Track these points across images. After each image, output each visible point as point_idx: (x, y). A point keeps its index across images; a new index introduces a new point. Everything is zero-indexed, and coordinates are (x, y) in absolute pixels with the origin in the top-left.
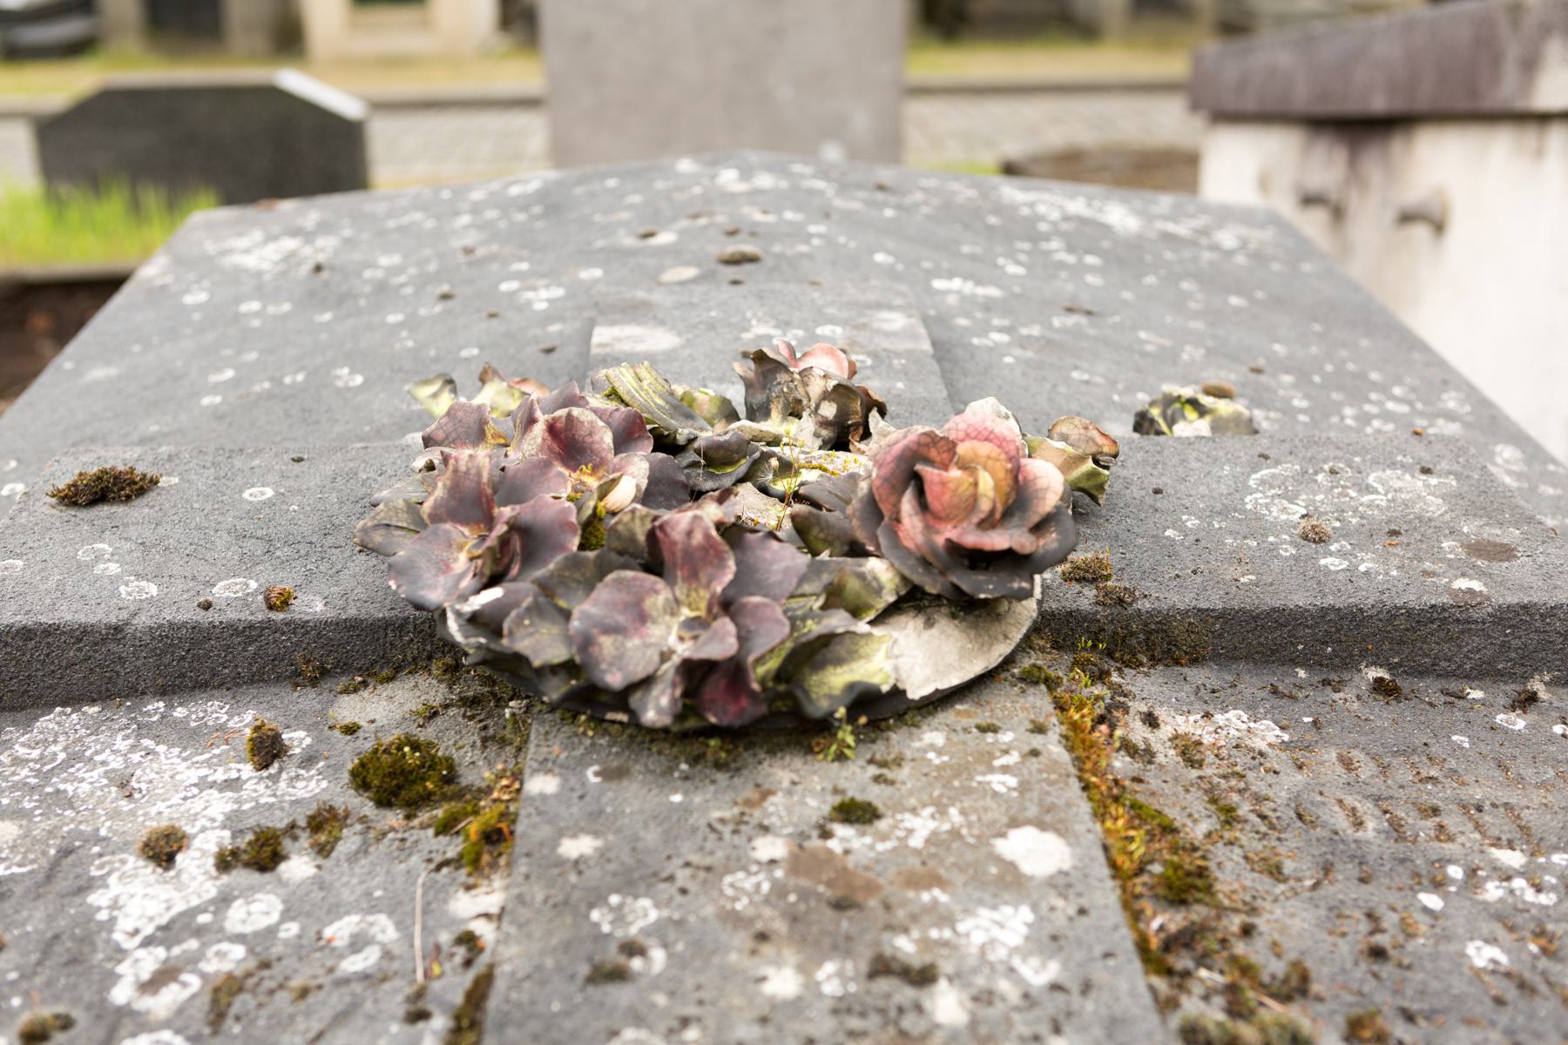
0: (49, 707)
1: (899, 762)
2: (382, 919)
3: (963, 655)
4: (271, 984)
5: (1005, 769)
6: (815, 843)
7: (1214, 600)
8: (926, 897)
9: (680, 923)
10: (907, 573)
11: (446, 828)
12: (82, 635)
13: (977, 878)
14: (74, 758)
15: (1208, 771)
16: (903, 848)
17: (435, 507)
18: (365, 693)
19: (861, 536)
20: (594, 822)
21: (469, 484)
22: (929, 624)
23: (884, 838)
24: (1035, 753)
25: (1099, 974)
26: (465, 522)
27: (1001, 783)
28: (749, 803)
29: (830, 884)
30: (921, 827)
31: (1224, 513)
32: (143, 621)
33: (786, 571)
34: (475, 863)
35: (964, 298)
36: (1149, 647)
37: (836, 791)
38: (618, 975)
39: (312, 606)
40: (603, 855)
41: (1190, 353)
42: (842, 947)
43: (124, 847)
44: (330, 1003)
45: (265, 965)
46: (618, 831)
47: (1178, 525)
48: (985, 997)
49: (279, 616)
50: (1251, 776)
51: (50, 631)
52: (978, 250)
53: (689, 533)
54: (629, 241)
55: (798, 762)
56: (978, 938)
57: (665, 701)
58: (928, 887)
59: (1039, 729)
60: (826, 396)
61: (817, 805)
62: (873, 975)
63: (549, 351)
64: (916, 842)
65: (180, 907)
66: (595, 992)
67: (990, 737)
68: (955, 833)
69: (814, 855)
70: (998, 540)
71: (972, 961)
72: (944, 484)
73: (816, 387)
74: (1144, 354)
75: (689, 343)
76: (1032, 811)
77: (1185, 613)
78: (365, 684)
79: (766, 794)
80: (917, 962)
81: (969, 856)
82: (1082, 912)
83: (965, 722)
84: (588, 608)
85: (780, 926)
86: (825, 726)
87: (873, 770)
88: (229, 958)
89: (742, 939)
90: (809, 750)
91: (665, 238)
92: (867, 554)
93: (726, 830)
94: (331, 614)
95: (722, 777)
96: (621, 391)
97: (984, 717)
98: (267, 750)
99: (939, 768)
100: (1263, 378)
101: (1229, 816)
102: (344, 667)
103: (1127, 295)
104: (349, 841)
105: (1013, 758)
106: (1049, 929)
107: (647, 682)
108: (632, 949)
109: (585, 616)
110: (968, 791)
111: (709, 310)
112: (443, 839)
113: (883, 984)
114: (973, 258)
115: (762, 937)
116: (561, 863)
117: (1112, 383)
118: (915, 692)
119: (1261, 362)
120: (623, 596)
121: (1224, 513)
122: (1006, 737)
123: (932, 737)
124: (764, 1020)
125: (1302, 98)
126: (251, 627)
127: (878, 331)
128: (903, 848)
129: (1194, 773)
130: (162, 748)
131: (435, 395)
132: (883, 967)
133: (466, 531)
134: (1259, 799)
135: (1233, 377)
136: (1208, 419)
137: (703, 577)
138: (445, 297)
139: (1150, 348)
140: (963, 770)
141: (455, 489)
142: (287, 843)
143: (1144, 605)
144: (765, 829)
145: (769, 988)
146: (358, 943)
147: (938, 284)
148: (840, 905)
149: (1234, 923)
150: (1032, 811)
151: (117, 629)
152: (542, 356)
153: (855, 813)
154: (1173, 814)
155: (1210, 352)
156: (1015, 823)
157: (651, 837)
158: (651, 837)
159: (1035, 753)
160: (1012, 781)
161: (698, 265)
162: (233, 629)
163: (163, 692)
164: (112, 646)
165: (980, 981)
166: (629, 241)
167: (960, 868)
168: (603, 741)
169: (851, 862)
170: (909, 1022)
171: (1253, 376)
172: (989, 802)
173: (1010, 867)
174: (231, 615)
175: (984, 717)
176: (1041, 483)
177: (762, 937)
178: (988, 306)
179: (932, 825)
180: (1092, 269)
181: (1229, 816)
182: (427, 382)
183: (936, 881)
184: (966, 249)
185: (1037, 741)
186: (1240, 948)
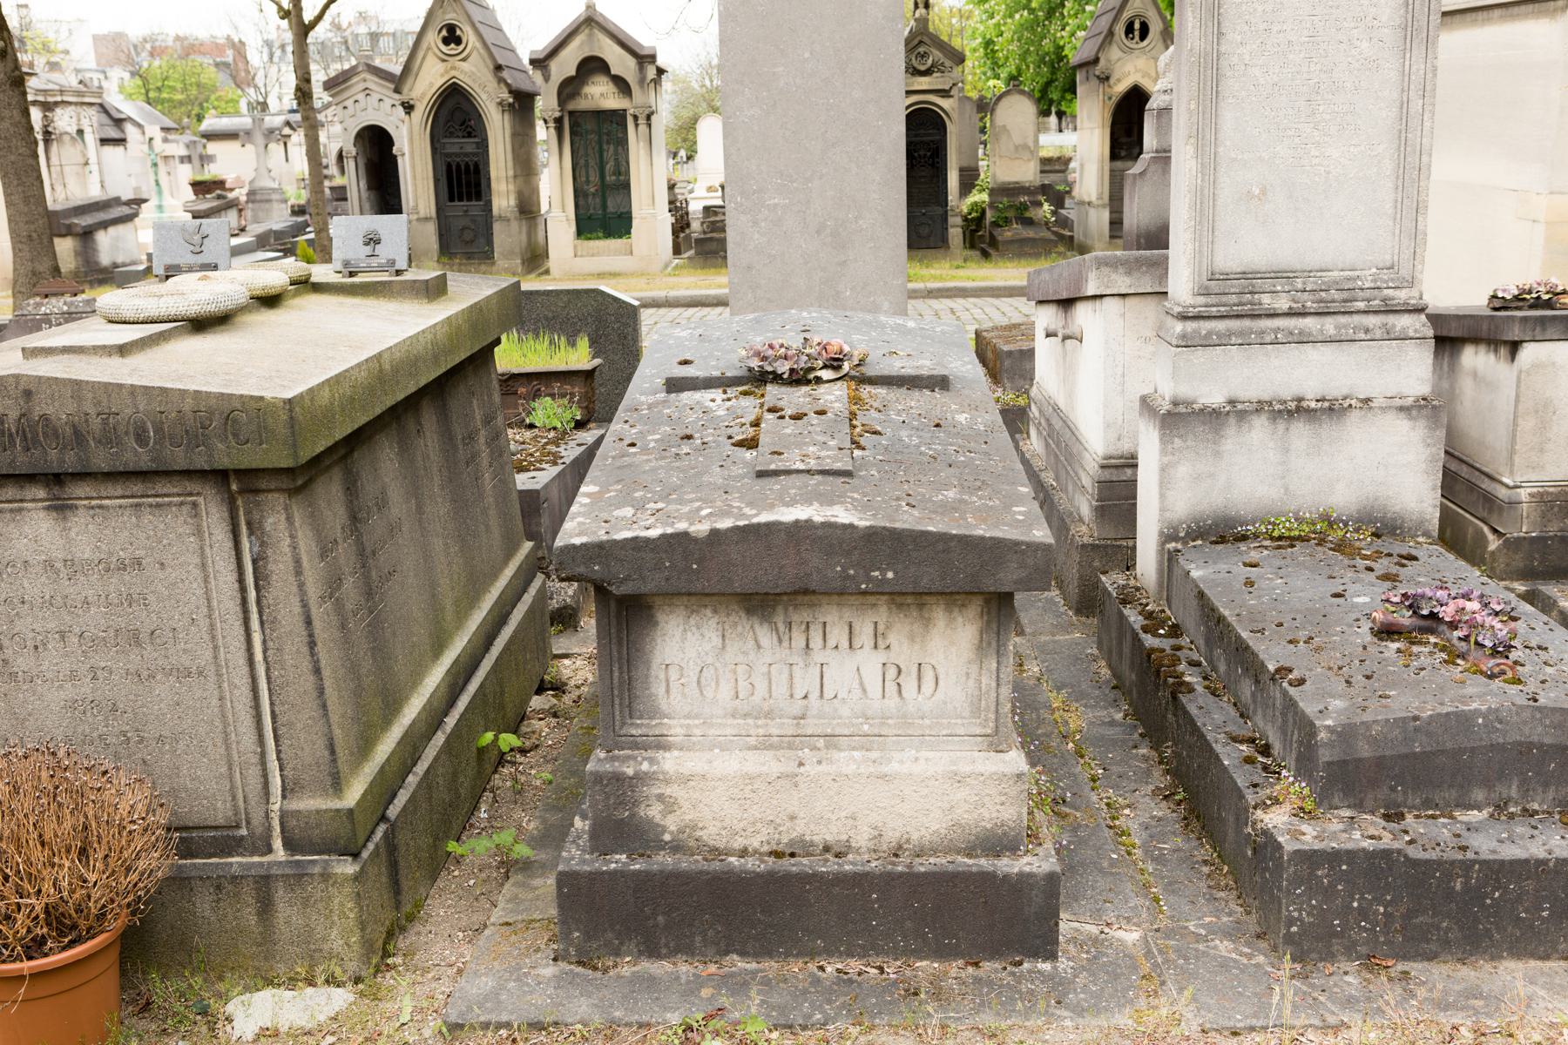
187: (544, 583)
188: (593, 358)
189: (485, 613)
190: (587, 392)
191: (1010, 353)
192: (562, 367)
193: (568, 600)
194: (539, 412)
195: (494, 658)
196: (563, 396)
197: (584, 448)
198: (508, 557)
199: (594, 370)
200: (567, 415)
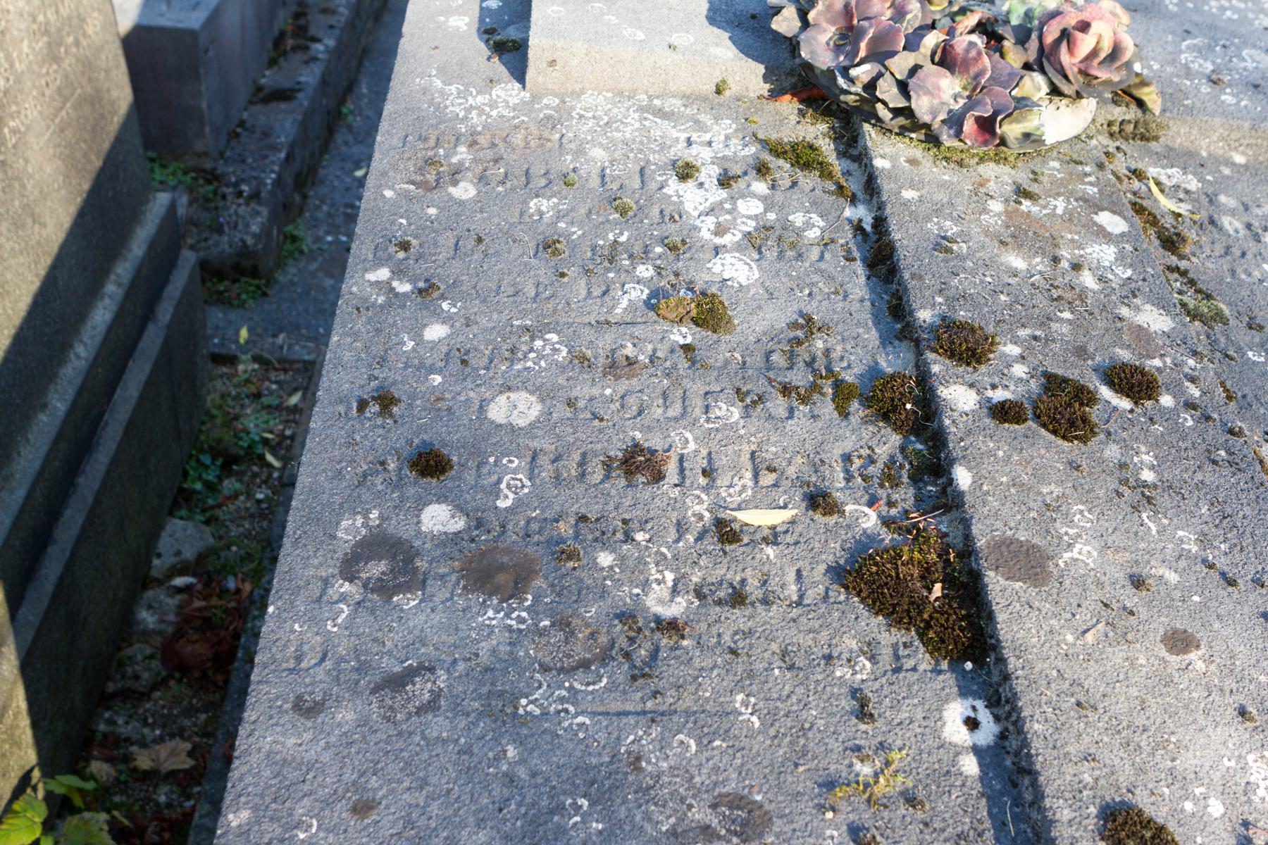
5: (1091, 184)
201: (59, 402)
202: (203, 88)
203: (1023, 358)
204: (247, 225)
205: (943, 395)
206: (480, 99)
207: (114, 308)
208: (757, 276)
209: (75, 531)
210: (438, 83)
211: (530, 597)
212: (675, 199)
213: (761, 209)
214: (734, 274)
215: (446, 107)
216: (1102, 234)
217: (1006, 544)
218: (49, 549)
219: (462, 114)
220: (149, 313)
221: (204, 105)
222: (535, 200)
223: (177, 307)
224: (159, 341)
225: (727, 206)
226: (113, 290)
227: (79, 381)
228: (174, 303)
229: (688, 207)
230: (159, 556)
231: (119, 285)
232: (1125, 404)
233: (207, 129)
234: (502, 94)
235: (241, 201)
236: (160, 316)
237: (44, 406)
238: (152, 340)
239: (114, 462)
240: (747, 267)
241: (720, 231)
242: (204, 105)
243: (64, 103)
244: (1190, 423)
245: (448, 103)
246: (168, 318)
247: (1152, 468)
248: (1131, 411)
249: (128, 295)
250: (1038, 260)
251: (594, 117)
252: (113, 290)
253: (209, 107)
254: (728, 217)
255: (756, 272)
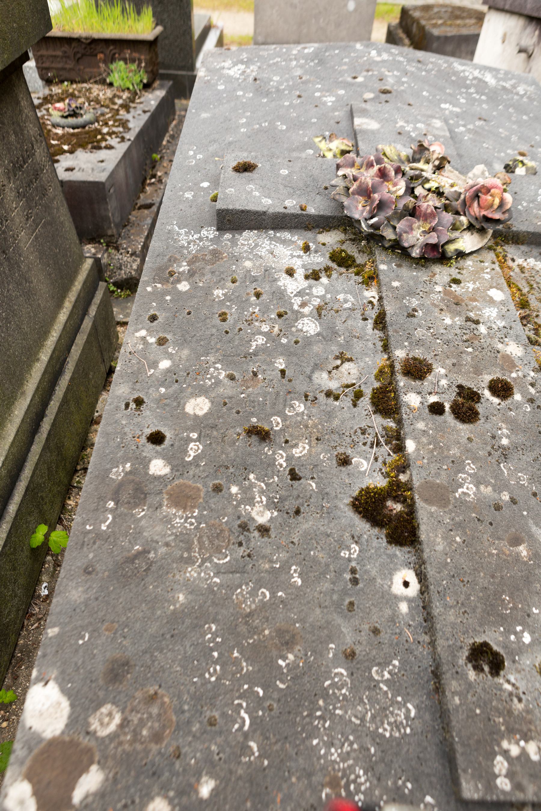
0: (245, 230)
1: (463, 269)
2: (349, 295)
3: (478, 242)
4: (328, 308)
5: (487, 273)
6: (448, 288)
7: (531, 229)
8: (474, 304)
9: (423, 305)
10: (470, 220)
11: (357, 274)
12: (256, 213)
13: (484, 300)
14: (256, 245)
15: (526, 275)
16: (467, 291)
17: (353, 191)
18: (324, 234)
19: (460, 210)
20: (398, 278)
21: (364, 186)
22: (472, 234)
23: (463, 288)
24: (493, 269)
25: (513, 325)
26: (361, 196)
27: (487, 276)
28: (431, 276)
29: (453, 298)
30: (471, 286)
31: (533, 201)
32: (271, 211)
33: (448, 221)
34: (367, 284)
35: (451, 112)
36: (512, 239)
37: (450, 275)
38: (413, 316)
39: (312, 210)
40: (402, 286)
41: (514, 138)
42: (459, 314)
43: (280, 271)
44: (344, 315)
45: (326, 304)
46: (404, 281)
47: (522, 205)
48: (490, 328)
49: (304, 213)
50: (536, 277)
51: (248, 212)
52: (451, 92)
53: (427, 209)
54: (349, 79)
55: (440, 267)
56: (487, 314)
57: (418, 251)
58: (475, 301)
59: (494, 263)
60: (437, 159)
61: (447, 279)
62: (466, 321)
63: (338, 123)
64: (470, 290)
65: (300, 288)
66: (409, 319)
67: (482, 264)
68: (478, 288)
69: (448, 291)
70: (497, 216)
71: (486, 320)
72: (486, 200)
73: (435, 156)
74: (502, 138)
75: (382, 127)
76: (495, 285)
77: (524, 232)
78: (323, 232)
79: (435, 274)
80: (475, 318)
81: (482, 294)
82: (508, 310)
83: (476, 259)
84: (401, 225)
85: (445, 308)
86: (451, 258)
87: (457, 271)
88: (317, 302)
89: (437, 310)
90: (442, 264)
91: (360, 79)
92: (461, 215)
93: (428, 283)
94: (317, 213)
95: (424, 269)
96: (387, 154)
97: (480, 258)
98: (306, 249)
99: (473, 271)
100: (534, 149)
101: (531, 287)
102: (318, 226)
103: (495, 113)
104: (334, 275)
105: (488, 270)
106: (501, 314)
107: (413, 246)
108: (415, 310)
109: (400, 228)
110: (480, 278)
111: (385, 114)
112: (357, 277)
113: (469, 323)
114: (450, 94)
115: (442, 310)
116: (393, 288)
117: (494, 149)
118: (467, 252)
119: (533, 143)
120: (408, 223)
121: (533, 201)
122: (486, 264)
123: (469, 263)
124: (446, 329)
125: (527, 11)
126: (297, 215)
127: (433, 127)
128: (467, 291)
129: (523, 275)
130: (278, 244)
131: (320, 141)
132: (468, 319)
133: (361, 198)
134: (538, 283)
135: (526, 148)
136: (524, 167)
137: (429, 221)
138: (299, 96)
139: (503, 135)
140: (477, 272)
141: (360, 186)
142: (320, 274)
143: (514, 229)
144: (436, 283)
145: (445, 322)
146: (346, 301)
147: (443, 106)
148: (457, 304)
149: (535, 314)
150: (495, 285)
151: (265, 212)
152: (336, 125)
153: (456, 281)
154: (521, 287)
155: (519, 138)
156: (491, 287)
157: (411, 283)
158: (411, 283)
159: (493, 269)
160: (489, 276)
161: (374, 93)
162: (293, 215)
163: (273, 229)
164: (263, 217)
165: (489, 324)
166: (349, 79)
167: (481, 297)
168: (394, 257)
169: (457, 293)
170: (475, 332)
171: (531, 148)
172: (485, 281)
173: (491, 298)
174: (293, 211)
175: (480, 258)
176: (507, 201)
177: (442, 310)
178: (457, 115)
179: (473, 286)
180: (483, 101)
181: (531, 287)
182: (317, 137)
183: (475, 300)
184: (448, 91)
185: (493, 266)
186: (536, 320)
187: (47, 536)
188: (157, 25)
189: (28, 400)
190: (151, 58)
191: (438, 38)
192: (131, 36)
193: (133, 273)
194: (116, 75)
195: (45, 436)
196: (133, 61)
197: (148, 114)
198: (59, 305)
199: (156, 39)
200: (137, 79)
201: (44, 356)
202: (109, 207)
203: (446, 375)
204: (131, 266)
205: (404, 400)
206: (196, 236)
207: (68, 313)
208: (319, 330)
209: (55, 411)
210: (177, 228)
211: (197, 511)
212: (283, 288)
213: (323, 293)
214: (308, 329)
215: (179, 241)
216: (491, 301)
217: (428, 485)
218: (44, 419)
219: (186, 245)
220: (85, 312)
221: (110, 215)
222: (217, 291)
223: (98, 308)
224: (90, 324)
225: (308, 291)
226: (68, 305)
227: (53, 347)
228: (97, 306)
229: (289, 291)
230: (97, 412)
231: (71, 302)
232: (496, 400)
233: (112, 225)
234: (206, 233)
235: (128, 255)
236: (91, 312)
237: (38, 360)
238: (87, 324)
239: (72, 379)
240: (314, 325)
241: (303, 305)
242: (110, 215)
243: (37, 227)
244: (529, 410)
245: (180, 238)
246: (94, 313)
247: (508, 437)
248: (499, 404)
249: (74, 307)
250: (457, 318)
251: (248, 244)
252: (68, 305)
253: (113, 215)
254: (307, 297)
255: (319, 328)
